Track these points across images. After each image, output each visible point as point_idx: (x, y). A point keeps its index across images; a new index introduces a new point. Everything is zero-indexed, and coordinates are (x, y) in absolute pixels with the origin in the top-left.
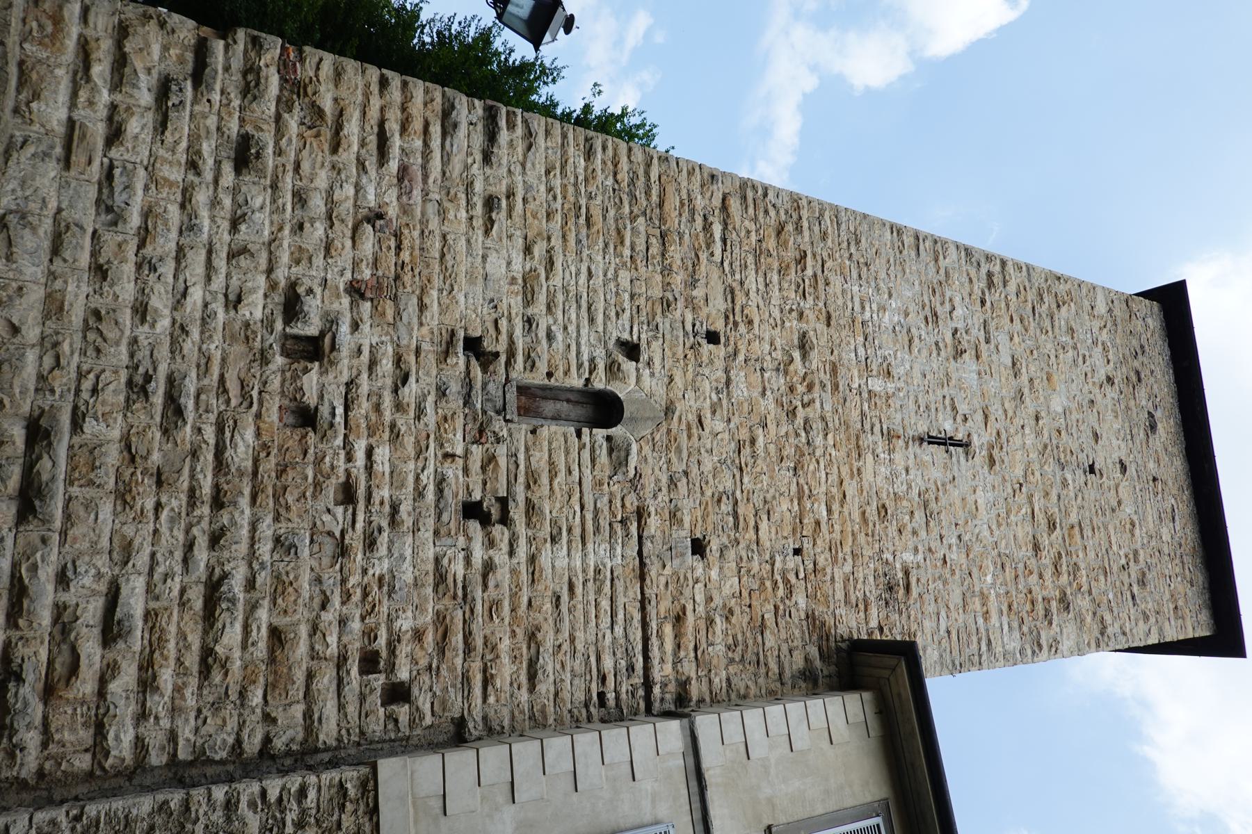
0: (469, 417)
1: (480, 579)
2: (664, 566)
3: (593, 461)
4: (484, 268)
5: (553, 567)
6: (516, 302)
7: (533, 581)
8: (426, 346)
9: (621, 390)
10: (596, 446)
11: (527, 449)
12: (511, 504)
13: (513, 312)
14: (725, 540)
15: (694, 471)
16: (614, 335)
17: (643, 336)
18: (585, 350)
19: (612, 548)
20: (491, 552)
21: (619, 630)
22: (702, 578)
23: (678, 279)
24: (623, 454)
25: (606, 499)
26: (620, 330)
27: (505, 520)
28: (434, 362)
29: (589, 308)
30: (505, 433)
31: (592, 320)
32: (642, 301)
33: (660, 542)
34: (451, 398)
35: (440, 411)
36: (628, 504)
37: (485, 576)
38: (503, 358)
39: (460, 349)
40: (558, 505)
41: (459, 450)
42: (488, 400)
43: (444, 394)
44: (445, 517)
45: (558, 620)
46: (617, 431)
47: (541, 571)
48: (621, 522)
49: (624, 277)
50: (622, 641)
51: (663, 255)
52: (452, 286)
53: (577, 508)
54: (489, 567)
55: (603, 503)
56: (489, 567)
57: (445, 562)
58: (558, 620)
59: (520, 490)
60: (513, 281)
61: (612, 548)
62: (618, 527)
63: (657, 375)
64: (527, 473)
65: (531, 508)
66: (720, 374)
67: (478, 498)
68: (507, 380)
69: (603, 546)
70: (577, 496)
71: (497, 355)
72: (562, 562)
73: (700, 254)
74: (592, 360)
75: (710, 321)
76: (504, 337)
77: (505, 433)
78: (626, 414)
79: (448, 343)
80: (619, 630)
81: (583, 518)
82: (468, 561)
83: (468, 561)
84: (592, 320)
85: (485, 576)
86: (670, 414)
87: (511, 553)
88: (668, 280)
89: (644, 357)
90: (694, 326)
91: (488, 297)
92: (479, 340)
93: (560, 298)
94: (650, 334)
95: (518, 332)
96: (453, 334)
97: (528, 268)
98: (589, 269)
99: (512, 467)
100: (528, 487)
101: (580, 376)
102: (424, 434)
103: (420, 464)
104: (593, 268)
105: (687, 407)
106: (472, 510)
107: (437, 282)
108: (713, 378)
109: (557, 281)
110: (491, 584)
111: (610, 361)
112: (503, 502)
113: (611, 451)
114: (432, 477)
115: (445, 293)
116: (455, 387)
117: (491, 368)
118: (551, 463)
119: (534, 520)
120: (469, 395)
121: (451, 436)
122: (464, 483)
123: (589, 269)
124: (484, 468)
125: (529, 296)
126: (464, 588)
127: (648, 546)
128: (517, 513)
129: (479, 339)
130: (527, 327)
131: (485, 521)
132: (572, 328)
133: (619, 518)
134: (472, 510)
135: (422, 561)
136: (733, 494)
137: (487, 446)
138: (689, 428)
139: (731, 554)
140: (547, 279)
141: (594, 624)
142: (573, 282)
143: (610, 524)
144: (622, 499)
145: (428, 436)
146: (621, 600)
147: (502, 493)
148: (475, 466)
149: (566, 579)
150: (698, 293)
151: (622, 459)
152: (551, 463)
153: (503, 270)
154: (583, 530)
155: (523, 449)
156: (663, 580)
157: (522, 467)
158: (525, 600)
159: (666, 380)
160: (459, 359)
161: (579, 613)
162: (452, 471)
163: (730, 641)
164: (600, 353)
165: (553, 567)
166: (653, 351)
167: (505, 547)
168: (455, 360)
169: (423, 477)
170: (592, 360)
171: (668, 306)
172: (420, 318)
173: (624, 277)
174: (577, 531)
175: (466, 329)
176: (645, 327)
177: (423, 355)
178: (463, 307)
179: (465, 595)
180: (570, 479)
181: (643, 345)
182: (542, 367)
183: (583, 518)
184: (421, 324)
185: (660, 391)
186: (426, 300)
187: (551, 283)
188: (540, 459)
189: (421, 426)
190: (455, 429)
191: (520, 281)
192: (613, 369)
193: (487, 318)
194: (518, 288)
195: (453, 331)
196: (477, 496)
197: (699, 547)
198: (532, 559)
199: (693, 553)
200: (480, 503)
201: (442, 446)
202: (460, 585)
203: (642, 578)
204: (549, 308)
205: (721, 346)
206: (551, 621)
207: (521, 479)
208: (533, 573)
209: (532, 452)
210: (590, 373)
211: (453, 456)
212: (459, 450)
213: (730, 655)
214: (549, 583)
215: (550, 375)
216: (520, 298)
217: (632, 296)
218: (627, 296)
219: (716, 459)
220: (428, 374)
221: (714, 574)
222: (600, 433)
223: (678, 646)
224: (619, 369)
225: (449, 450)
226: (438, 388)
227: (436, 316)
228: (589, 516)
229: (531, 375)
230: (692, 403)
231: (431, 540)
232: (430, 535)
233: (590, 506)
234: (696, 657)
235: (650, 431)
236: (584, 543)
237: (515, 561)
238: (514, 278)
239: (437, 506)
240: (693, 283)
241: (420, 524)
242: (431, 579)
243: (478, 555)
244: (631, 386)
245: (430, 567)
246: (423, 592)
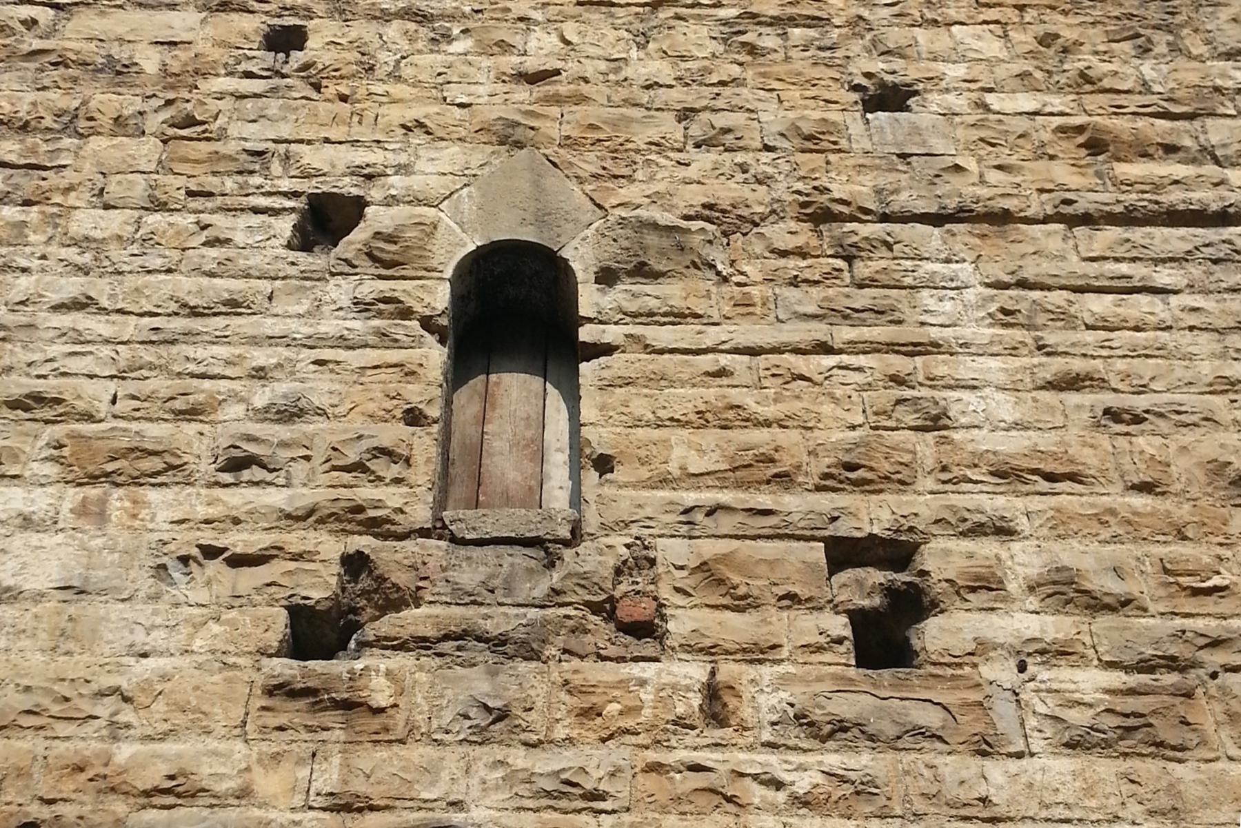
0: (573, 644)
1: (1104, 621)
2: (958, 168)
3: (678, 317)
4: (39, 597)
5: (1017, 426)
6: (163, 504)
7: (1073, 477)
8: (328, 777)
9: (455, 243)
10: (632, 307)
11: (664, 481)
12: (843, 529)
13: (202, 511)
14: (856, 47)
15: (678, 96)
16: (283, 252)
17: (286, 185)
18: (330, 326)
19: (931, 284)
20: (1013, 587)
21: (1165, 276)
22: (974, 96)
23: (105, 101)
24: (652, 239)
25: (791, 294)
26: (267, 239)
27: (895, 551)
28: (382, 753)
29: (195, 312)
30: (619, 541)
31: (234, 306)
32: (174, 185)
33: (892, 177)
34: (513, 692)
35: (560, 732)
36: (791, 243)
37: (1096, 605)
38: (363, 542)
39: (338, 667)
40: (827, 409)
41: (695, 672)
42: (509, 590)
43: (502, 715)
44: (931, 718)
45: (1180, 419)
46: (581, 258)
47: (1036, 452)
48: (849, 259)
49: (87, 221)
50: (1196, 271)
51: (25, 127)
52: (101, 694)
53: (831, 360)
54: (1062, 590)
55: (810, 299)
56: (1062, 590)
57: (1077, 717)
58: (1180, 419)
59: (794, 503)
60: (94, 513)
61: (931, 284)
62: (863, 269)
63: (403, 159)
64: (740, 485)
65: (848, 474)
66: (393, 30)
67: (844, 619)
68: (437, 530)
69: (932, 304)
70: (800, 364)
71: (355, 564)
72: (1005, 408)
73: (25, 48)
74: (362, 307)
75: (240, 42)
76: (295, 539)
77: (619, 541)
78: (528, 234)
79: (317, 708)
80: (1165, 276)
81: (854, 347)
82: (1058, 653)
83: (1058, 653)
84: (234, 306)
85: (1096, 605)
86: (519, 134)
87: (1003, 531)
88: (105, 121)
89: (348, 186)
90: (249, 75)
91: (146, 584)
92: (299, 614)
93: (159, 384)
94: (276, 167)
95: (276, 498)
96: (281, 690)
97: (51, 470)
98: (59, 308)
99: (726, 523)
100: (784, 480)
101: (416, 343)
102: (650, 782)
103: (758, 793)
104: (55, 298)
105: (490, 97)
106: (883, 639)
107: (84, 743)
108: (405, 45)
109: (97, 394)
110: (1116, 587)
111: (365, 264)
112: (845, 553)
113: (642, 271)
114: (796, 758)
115: (127, 715)
116: (479, 682)
117: (401, 578)
118: (703, 419)
119: (886, 467)
120: (498, 643)
121: (647, 695)
122: (800, 659)
123: (59, 308)
124: (743, 604)
125: (156, 464)
126: (1145, 666)
127: (904, 200)
128: (871, 516)
129: (299, 614)
130: (257, 473)
131: (912, 604)
132: (261, 357)
133: (840, 263)
134: (883, 639)
135: (1089, 792)
136: (725, 23)
137: (665, 593)
138: (557, 100)
139: (895, 36)
140: (89, 417)
141: (1164, 336)
142: (106, 351)
143: (861, 286)
144: (784, 254)
145: (655, 768)
146: (1074, 264)
147: (817, 553)
148: (737, 627)
149: (1047, 396)
150: (150, 61)
151: (666, 242)
152: (703, 419)
153: (50, 540)
154: (892, 347)
155: (665, 494)
156: (994, 176)
157: (726, 497)
158: (1140, 501)
159: (418, 138)
160: (376, 673)
161: (1146, 368)
162: (764, 695)
163: (1127, 46)
164: (340, 291)
165: (1017, 426)
166: (331, 166)
167: (987, 547)
168: (378, 682)
169: (802, 783)
170: (362, 307)
171: (190, 122)
172: (218, 801)
173: (87, 221)
174: (899, 364)
175: (263, 652)
176: (256, 180)
177: (359, 786)
178: (184, 662)
179: (1172, 664)
180: (742, 376)
181: (308, 186)
182: (392, 434)
183: (854, 347)
184: (244, 794)
185: (451, 156)
186: (154, 776)
187: (103, 408)
188: (691, 451)
189: (620, 790)
190: (622, 684)
191: (93, 492)
192: (388, 258)
193: (223, 590)
194: (118, 501)
195: (270, 692)
196: (839, 625)
197: (889, 97)
198: (1007, 474)
199: (907, 109)
200: (858, 618)
201: (681, 723)
202: (1135, 680)
203: (1003, 218)
204: (192, 413)
205: (310, 24)
206: (1188, 437)
207: (764, 500)
208: (1051, 477)
209: (673, 468)
210: (406, 314)
211: (713, 692)
212: (695, 672)
213: (1162, 49)
214: (1069, 429)
215: (414, 417)
216: (153, 495)
217: (160, 206)
218: (154, 220)
219: (634, 53)
220: (430, 771)
221: (956, 72)
222: (589, 299)
223: (1170, 149)
224: (391, 239)
225: (696, 700)
226: (481, 738)
227: (212, 743)
228: (845, 333)
229: (419, 458)
230: (481, 90)
231: (1013, 765)
232: (997, 770)
233: (819, 331)
234: (1191, 117)
235: (573, 185)
236: (934, 347)
237: (1023, 524)
238: (82, 510)
239: (893, 744)
240: (120, 72)
241: (964, 795)
242: (1148, 768)
243: (1025, 622)
244: (449, 206)
245: (1105, 768)
246: (1193, 792)
